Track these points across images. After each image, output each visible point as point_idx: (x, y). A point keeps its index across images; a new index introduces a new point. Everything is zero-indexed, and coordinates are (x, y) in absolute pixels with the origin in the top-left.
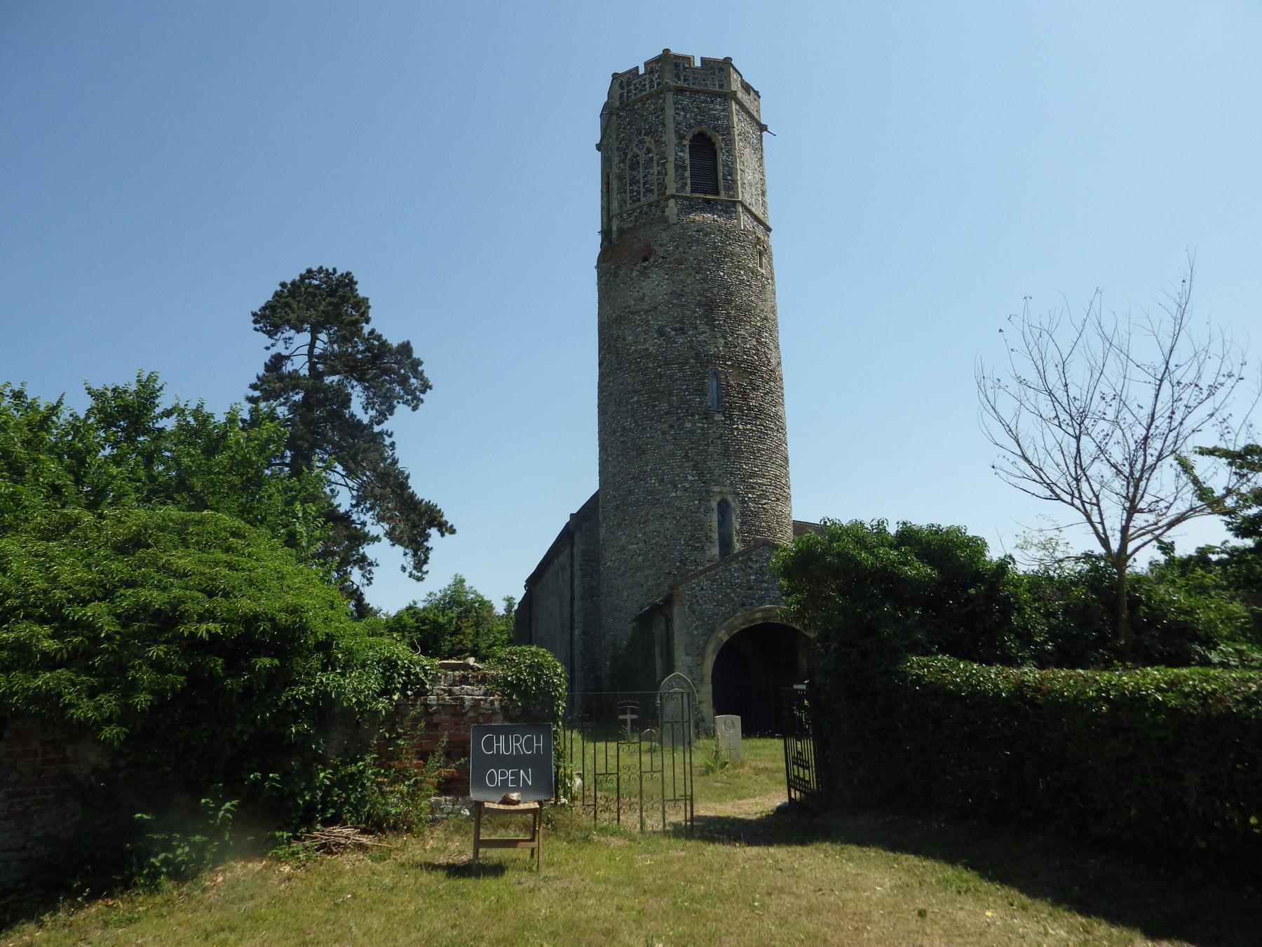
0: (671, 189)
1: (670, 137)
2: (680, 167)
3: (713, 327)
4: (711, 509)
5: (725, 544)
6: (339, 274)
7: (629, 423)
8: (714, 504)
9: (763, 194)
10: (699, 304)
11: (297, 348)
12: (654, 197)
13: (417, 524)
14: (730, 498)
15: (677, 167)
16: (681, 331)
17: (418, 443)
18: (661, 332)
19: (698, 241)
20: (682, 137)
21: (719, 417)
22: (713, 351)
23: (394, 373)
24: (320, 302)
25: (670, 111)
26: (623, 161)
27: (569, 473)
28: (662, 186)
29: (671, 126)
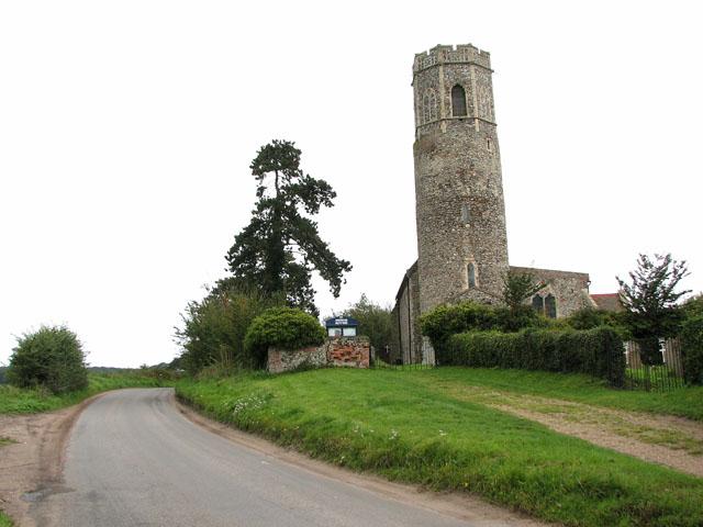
0: (443, 116)
1: (443, 91)
2: (447, 104)
3: (464, 183)
4: (301, 276)
5: (471, 284)
6: (322, 206)
7: (427, 229)
9: (492, 107)
10: (457, 172)
11: (272, 183)
12: (436, 119)
13: (333, 269)
14: (474, 263)
15: (446, 104)
16: (450, 186)
17: (329, 224)
18: (440, 187)
19: (456, 141)
20: (447, 89)
21: (468, 226)
22: (464, 193)
23: (316, 192)
24: (278, 157)
25: (441, 76)
26: (421, 100)
27: (405, 251)
28: (439, 113)
29: (442, 86)
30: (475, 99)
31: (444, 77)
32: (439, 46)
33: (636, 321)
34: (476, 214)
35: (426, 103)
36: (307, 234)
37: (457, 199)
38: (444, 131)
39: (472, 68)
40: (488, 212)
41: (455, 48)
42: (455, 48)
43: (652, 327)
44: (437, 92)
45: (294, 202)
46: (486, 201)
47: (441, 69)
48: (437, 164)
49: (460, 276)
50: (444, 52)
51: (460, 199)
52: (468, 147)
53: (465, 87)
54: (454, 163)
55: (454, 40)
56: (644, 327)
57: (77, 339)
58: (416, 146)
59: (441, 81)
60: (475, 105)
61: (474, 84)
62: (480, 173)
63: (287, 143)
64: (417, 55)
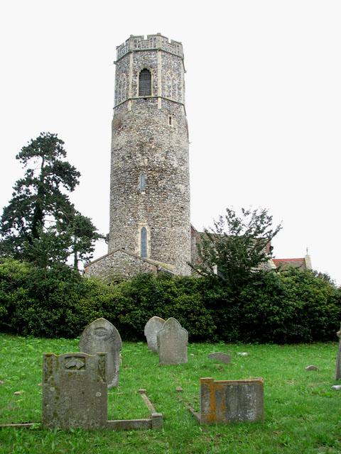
1: (131, 74)
8: (139, 230)
11: (36, 164)
14: (146, 227)
16: (130, 157)
20: (135, 73)
21: (143, 193)
22: (142, 164)
24: (46, 146)
25: (131, 62)
29: (131, 70)
30: (160, 81)
31: (133, 63)
32: (132, 37)
33: (211, 288)
34: (152, 183)
35: (120, 86)
36: (64, 206)
37: (147, 175)
38: (130, 109)
39: (160, 54)
40: (165, 181)
41: (146, 38)
42: (146, 38)
43: (231, 296)
44: (128, 76)
45: (57, 183)
46: (162, 171)
47: (131, 55)
48: (123, 139)
49: (133, 240)
50: (135, 41)
51: (139, 169)
52: (148, 122)
53: (151, 70)
54: (135, 136)
55: (144, 31)
56: (216, 296)
57: (284, 249)
58: (113, 122)
59: (131, 66)
60: (160, 86)
61: (160, 67)
62: (159, 146)
63: (53, 135)
64: (118, 47)
